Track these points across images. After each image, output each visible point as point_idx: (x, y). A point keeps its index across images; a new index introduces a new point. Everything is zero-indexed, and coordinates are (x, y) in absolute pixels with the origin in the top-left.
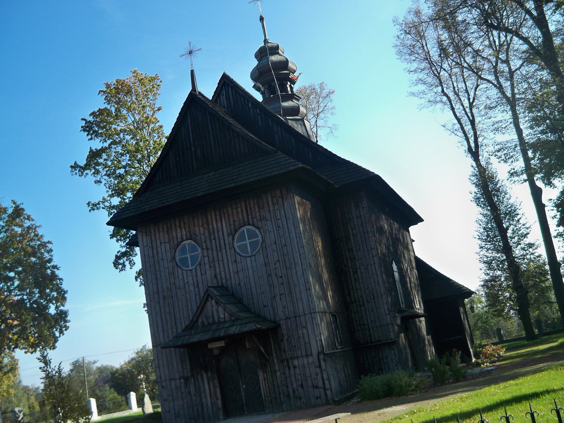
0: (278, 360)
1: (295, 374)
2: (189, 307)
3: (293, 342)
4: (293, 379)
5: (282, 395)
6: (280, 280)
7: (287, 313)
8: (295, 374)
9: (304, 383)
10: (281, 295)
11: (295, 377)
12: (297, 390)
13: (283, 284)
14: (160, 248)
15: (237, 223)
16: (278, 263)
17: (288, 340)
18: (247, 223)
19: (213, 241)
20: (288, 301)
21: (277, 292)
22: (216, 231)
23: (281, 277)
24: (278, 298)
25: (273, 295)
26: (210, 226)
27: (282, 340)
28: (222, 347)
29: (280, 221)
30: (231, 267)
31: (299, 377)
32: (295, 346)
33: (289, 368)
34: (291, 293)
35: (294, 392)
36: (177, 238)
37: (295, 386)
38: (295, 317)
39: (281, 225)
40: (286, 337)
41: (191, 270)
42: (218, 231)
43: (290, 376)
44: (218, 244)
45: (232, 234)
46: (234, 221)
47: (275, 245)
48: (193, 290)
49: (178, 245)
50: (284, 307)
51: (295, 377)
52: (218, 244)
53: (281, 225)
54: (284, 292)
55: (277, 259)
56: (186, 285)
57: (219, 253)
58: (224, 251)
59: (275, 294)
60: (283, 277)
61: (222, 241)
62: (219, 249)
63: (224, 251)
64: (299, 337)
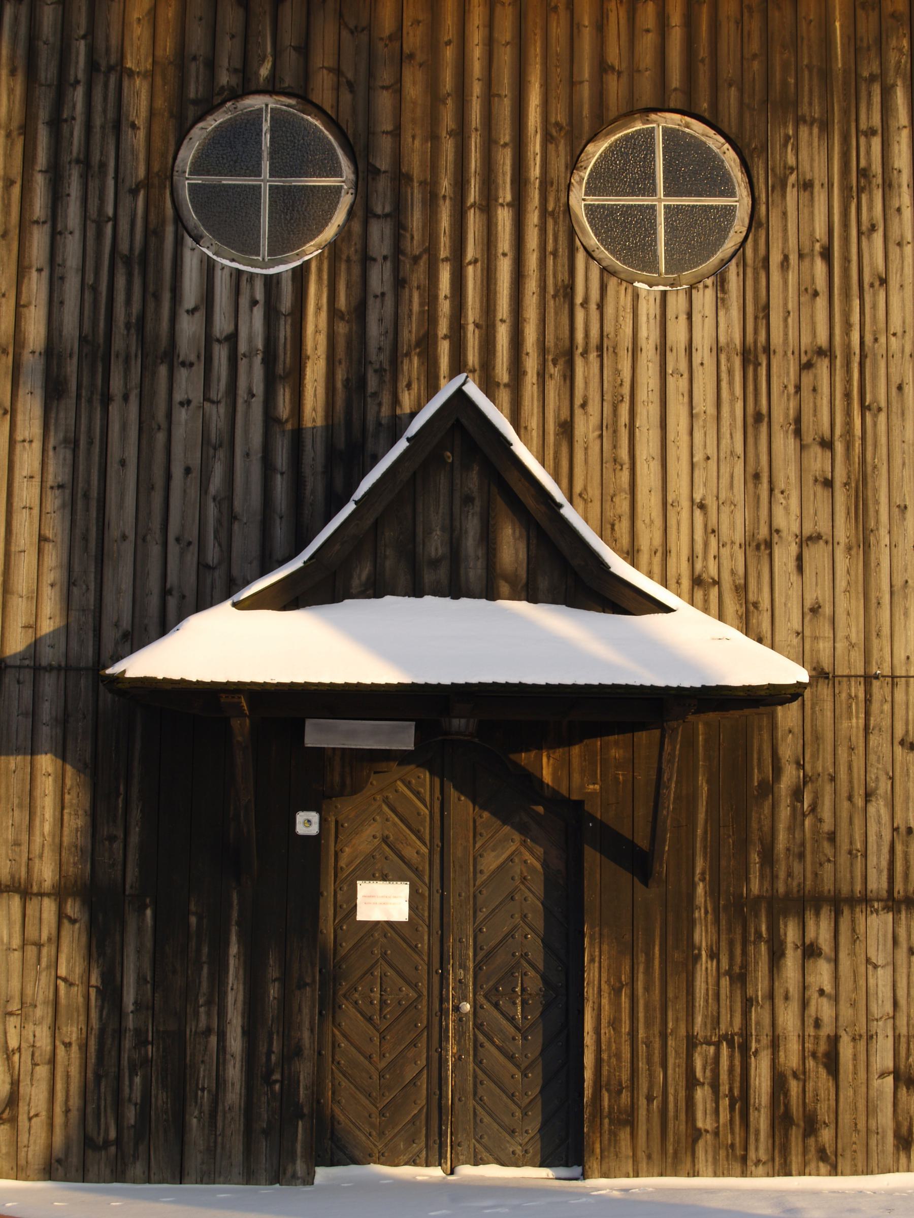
0: (714, 892)
1: (804, 988)
2: (216, 482)
3: (826, 813)
4: (789, 1018)
5: (701, 1095)
6: (818, 461)
7: (824, 647)
8: (804, 988)
9: (846, 1050)
10: (806, 540)
11: (804, 1004)
12: (801, 1075)
13: (828, 484)
14: (79, 94)
15: (615, 87)
16: (823, 366)
17: (797, 794)
18: (675, 100)
19: (448, 147)
20: (841, 584)
21: (787, 520)
22: (477, 89)
23: (827, 444)
24: (785, 555)
25: (764, 532)
26: (449, 54)
27: (768, 789)
28: (332, 1163)
29: (876, 142)
30: (531, 313)
31: (826, 1010)
32: (832, 837)
33: (776, 956)
34: (867, 546)
35: (779, 1081)
36: (211, 65)
37: (791, 1057)
38: (868, 679)
39: (877, 168)
40: (789, 776)
41: (271, 89)
42: (489, 97)
43: (771, 996)
44: (474, 162)
45: (571, 138)
46: (602, 67)
47: (820, 267)
48: (259, 388)
49: (208, 108)
50: (815, 610)
51: (804, 1004)
52: (474, 162)
53: (877, 168)
54: (824, 527)
55: (822, 339)
56: (221, 354)
57: (474, 221)
58: (504, 218)
59: (774, 531)
60: (839, 447)
61: (505, 161)
62: (473, 194)
63: (504, 218)
64: (692, 1083)
